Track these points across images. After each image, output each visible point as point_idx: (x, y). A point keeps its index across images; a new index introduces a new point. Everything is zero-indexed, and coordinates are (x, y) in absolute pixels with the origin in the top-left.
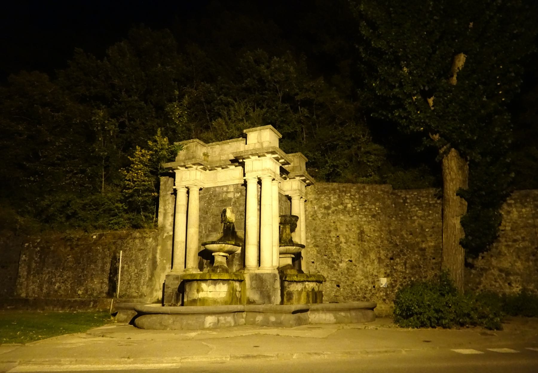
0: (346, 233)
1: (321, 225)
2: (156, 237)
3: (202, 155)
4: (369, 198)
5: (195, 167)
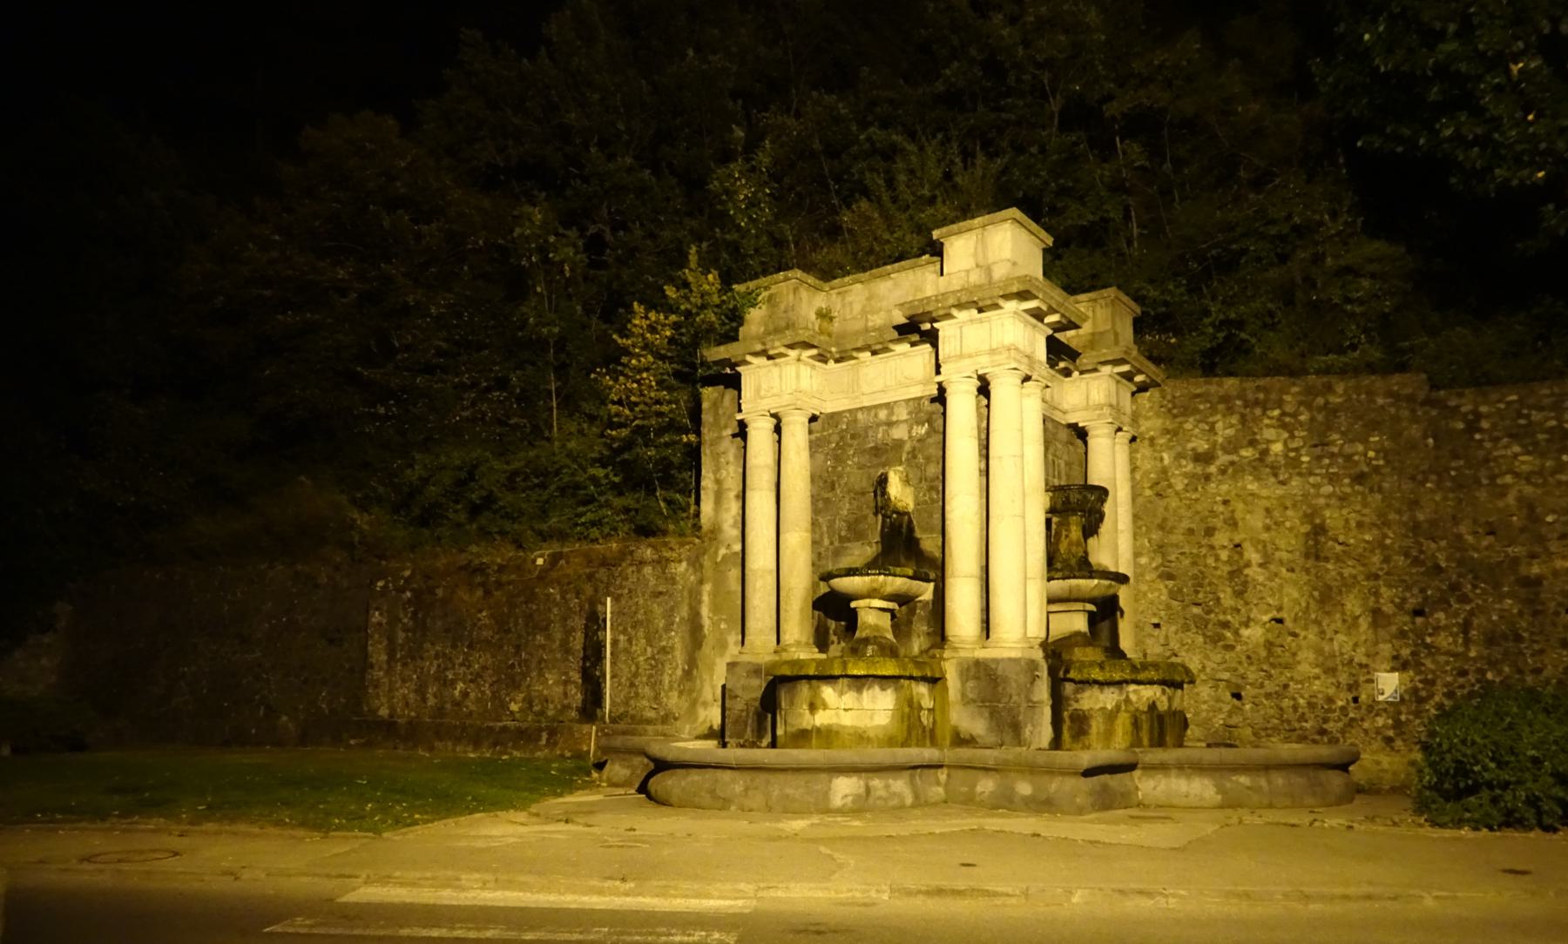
0: (1265, 536)
1: (1182, 511)
2: (697, 557)
3: (813, 317)
5: (793, 353)
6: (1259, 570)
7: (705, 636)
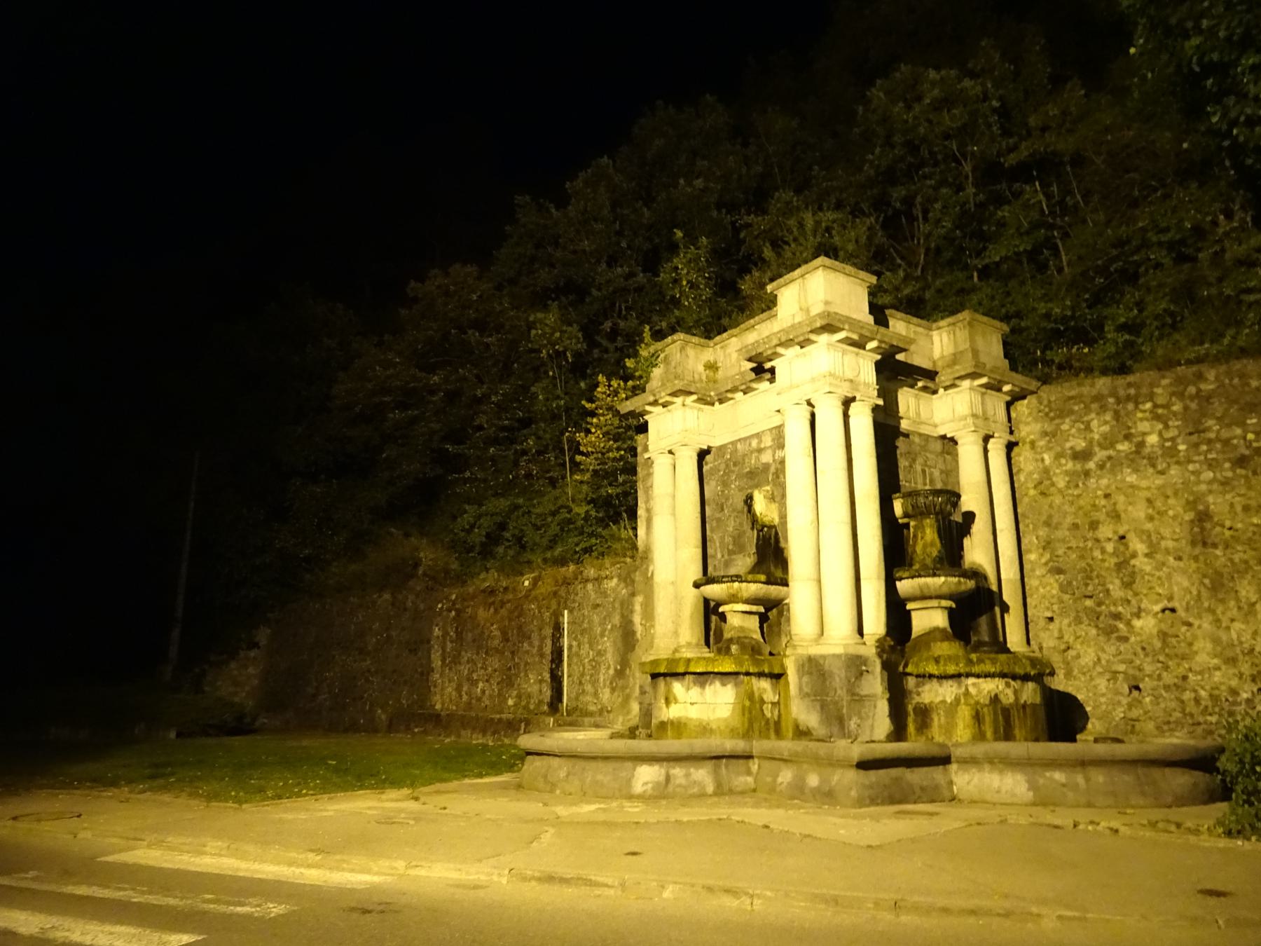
0: (1149, 526)
1: (1066, 507)
2: (629, 574)
3: (701, 368)
4: (1218, 407)
5: (679, 400)
6: (1146, 560)
7: (638, 640)
